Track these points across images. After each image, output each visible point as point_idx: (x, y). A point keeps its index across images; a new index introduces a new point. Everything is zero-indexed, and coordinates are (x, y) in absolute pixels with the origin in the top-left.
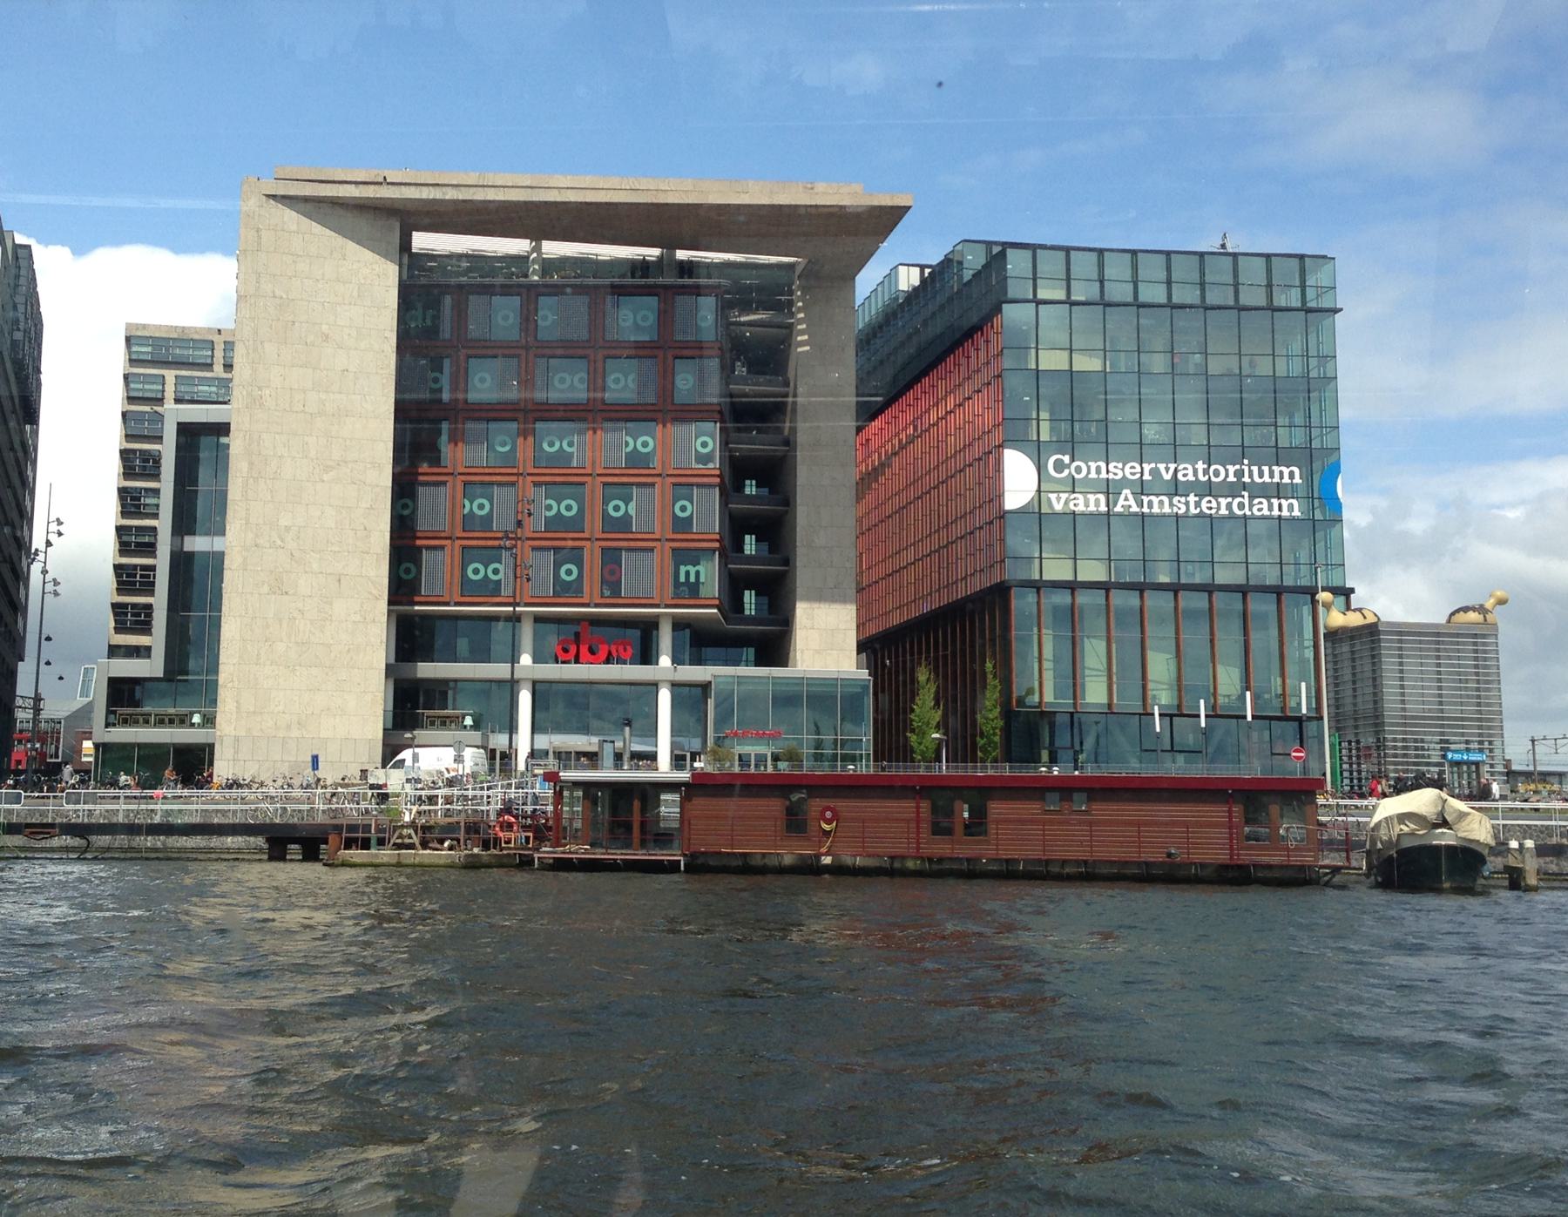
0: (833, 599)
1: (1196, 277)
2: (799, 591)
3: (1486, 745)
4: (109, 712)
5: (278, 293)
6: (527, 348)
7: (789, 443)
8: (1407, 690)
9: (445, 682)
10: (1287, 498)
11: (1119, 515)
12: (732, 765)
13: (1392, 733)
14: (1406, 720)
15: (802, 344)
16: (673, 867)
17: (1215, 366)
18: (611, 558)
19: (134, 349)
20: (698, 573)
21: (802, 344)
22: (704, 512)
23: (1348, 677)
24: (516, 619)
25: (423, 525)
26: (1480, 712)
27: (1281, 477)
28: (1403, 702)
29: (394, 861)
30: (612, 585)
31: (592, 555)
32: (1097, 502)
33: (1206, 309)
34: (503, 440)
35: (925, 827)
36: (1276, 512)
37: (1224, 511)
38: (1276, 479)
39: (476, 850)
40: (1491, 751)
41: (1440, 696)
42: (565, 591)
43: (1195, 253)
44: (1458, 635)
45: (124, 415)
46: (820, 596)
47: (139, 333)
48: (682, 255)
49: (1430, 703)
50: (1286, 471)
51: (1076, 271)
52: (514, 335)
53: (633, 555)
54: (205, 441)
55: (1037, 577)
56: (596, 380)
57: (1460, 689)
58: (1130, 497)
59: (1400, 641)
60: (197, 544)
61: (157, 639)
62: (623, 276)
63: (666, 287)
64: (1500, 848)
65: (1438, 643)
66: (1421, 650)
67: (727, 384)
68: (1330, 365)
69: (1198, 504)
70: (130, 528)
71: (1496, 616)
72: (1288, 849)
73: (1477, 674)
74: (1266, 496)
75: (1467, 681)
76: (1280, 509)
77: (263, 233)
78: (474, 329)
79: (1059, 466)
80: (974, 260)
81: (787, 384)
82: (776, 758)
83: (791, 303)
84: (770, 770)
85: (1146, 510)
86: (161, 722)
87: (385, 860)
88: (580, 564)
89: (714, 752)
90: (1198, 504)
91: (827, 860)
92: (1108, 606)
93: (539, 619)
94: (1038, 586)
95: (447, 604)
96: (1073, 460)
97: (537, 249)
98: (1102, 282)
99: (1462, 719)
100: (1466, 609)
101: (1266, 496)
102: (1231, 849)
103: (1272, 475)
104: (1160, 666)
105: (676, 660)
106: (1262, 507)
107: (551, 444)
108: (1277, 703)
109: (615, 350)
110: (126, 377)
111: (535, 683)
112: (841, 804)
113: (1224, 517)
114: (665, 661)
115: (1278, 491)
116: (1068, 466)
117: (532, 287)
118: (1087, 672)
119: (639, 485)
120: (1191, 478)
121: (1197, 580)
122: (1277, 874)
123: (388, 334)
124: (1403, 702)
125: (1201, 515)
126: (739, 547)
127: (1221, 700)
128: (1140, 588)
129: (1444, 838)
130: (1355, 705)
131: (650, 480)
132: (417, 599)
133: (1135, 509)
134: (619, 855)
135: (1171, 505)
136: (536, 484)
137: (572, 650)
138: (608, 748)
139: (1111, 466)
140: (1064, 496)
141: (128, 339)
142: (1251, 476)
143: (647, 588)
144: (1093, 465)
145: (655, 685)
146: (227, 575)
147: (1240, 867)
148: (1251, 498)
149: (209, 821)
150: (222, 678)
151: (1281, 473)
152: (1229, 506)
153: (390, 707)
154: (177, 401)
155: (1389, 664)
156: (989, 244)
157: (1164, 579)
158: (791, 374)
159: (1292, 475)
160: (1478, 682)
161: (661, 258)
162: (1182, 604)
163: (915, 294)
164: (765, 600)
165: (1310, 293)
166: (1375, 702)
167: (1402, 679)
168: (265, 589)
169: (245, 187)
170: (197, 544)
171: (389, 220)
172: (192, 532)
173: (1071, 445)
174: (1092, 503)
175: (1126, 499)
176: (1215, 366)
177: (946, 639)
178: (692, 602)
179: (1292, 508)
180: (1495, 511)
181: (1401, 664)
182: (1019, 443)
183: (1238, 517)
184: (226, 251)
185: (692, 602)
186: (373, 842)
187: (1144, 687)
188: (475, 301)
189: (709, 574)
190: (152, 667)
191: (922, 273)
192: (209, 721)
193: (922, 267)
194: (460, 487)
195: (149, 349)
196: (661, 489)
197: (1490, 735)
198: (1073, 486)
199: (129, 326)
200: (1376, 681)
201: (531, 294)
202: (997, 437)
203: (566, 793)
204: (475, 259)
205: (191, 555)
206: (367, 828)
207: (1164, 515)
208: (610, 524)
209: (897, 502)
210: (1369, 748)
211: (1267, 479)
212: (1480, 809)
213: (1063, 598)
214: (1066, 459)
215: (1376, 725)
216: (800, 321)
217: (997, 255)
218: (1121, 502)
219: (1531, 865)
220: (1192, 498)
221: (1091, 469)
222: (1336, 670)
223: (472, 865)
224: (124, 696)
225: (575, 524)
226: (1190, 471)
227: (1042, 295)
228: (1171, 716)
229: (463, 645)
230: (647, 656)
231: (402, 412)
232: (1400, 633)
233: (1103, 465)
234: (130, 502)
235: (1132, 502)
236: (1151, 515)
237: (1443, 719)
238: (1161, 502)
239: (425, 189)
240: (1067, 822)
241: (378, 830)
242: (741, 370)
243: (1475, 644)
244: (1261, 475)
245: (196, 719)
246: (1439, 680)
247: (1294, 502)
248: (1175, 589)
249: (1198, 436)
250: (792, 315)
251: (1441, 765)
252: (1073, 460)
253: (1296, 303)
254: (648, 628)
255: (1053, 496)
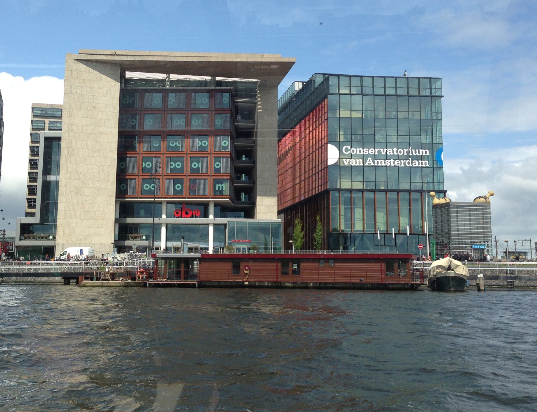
0: (269, 195)
1: (394, 85)
2: (258, 193)
3: (486, 243)
4: (21, 235)
5: (78, 93)
6: (164, 111)
7: (255, 142)
8: (459, 225)
9: (138, 224)
10: (424, 160)
11: (367, 166)
12: (234, 252)
13: (454, 239)
14: (459, 235)
15: (260, 109)
16: (194, 286)
17: (400, 116)
18: (193, 182)
19: (35, 112)
20: (222, 187)
21: (260, 109)
22: (225, 166)
23: (440, 220)
24: (161, 203)
25: (128, 171)
26: (484, 232)
27: (423, 153)
28: (458, 229)
29: (100, 285)
30: (193, 190)
31: (187, 183)
32: (360, 162)
33: (363, 95)
34: (156, 143)
35: (279, 272)
36: (420, 165)
37: (403, 165)
38: (421, 154)
39: (129, 281)
40: (488, 245)
41: (470, 226)
42: (178, 193)
43: (417, 78)
44: (477, 206)
45: (31, 134)
46: (266, 194)
47: (37, 107)
48: (218, 79)
49: (467, 229)
50: (424, 151)
51: (353, 83)
52: (160, 106)
53: (200, 181)
54: (55, 144)
55: (339, 188)
56: (188, 122)
57: (477, 224)
58: (371, 160)
59: (457, 208)
60: (52, 178)
61: (37, 210)
62: (198, 86)
63: (212, 90)
64: (473, 277)
65: (470, 209)
66: (464, 211)
67: (234, 123)
68: (439, 115)
69: (394, 163)
70: (33, 173)
71: (491, 199)
72: (400, 278)
73: (483, 219)
74: (416, 158)
75: (480, 221)
76: (422, 164)
77: (73, 72)
78: (147, 104)
79: (347, 150)
80: (319, 80)
81: (254, 123)
82: (249, 249)
83: (256, 95)
84: (247, 253)
85: (376, 164)
86: (38, 239)
87: (98, 284)
88: (182, 184)
89: (228, 247)
90: (394, 163)
91: (246, 283)
92: (363, 197)
93: (168, 203)
94: (339, 190)
95: (137, 198)
96: (351, 148)
97: (168, 77)
98: (373, 88)
99: (478, 234)
100: (480, 197)
101: (416, 158)
102: (381, 278)
103: (419, 152)
104: (381, 217)
105: (216, 216)
106: (416, 164)
107: (173, 144)
108: (420, 229)
109: (199, 112)
110: (32, 121)
111: (167, 225)
112: (250, 264)
113: (403, 167)
114: (211, 217)
115: (421, 158)
116: (350, 150)
117: (167, 90)
118: (356, 219)
119: (202, 157)
120: (392, 153)
121: (394, 188)
122: (396, 286)
123: (116, 106)
124: (458, 229)
125: (395, 166)
126: (239, 178)
127: (401, 229)
128: (374, 191)
129: (451, 274)
130: (442, 230)
131: (206, 155)
132: (126, 196)
133: (372, 164)
134: (175, 282)
135: (385, 163)
136: (167, 157)
137: (180, 213)
138: (186, 246)
139: (364, 150)
140: (348, 160)
141: (33, 108)
142: (412, 153)
143: (204, 192)
144: (358, 150)
145: (208, 225)
146: (60, 188)
147: (384, 284)
148: (412, 160)
149: (49, 272)
150: (58, 224)
151: (422, 152)
152: (405, 163)
153: (117, 232)
154: (50, 129)
155: (453, 216)
156: (324, 74)
157: (382, 188)
158: (256, 119)
159: (426, 152)
160: (483, 222)
161: (211, 80)
162: (388, 196)
163: (301, 91)
164: (247, 196)
165: (433, 91)
166: (448, 229)
167: (457, 221)
168: (73, 193)
169: (67, 57)
170: (52, 178)
171: (118, 68)
172: (50, 174)
173: (351, 143)
174: (358, 162)
175: (369, 161)
176: (400, 116)
177: (308, 210)
178: (220, 197)
179: (426, 164)
180: (511, 164)
181: (457, 216)
182: (333, 142)
183: (408, 167)
184: (60, 77)
185: (220, 197)
186: (95, 278)
187: (375, 224)
188: (147, 95)
189: (226, 187)
190: (35, 220)
191: (303, 84)
192: (54, 238)
193: (303, 82)
194: (141, 158)
195: (40, 112)
196: (210, 158)
197: (487, 240)
198: (351, 156)
199: (33, 104)
200: (449, 221)
201: (165, 92)
202: (326, 140)
203: (159, 261)
204: (147, 81)
205: (50, 182)
206: (92, 274)
207: (383, 166)
208: (192, 170)
209: (295, 162)
210: (446, 244)
211: (417, 154)
212: (464, 264)
213: (348, 195)
214: (349, 147)
215: (449, 236)
216: (259, 101)
217: (327, 77)
218: (368, 162)
219: (482, 283)
220: (392, 161)
221: (357, 151)
222: (436, 218)
223: (127, 286)
224: (26, 230)
225: (181, 170)
226: (391, 151)
227: (342, 91)
228: (384, 234)
229: (142, 212)
230: (206, 215)
231: (121, 134)
232: (457, 206)
233: (361, 149)
234: (33, 164)
235: (371, 162)
236: (378, 166)
237: (471, 234)
238: (381, 162)
239: (129, 57)
240: (326, 270)
241: (97, 274)
242: (239, 118)
243: (483, 209)
244: (416, 152)
245: (51, 237)
246: (470, 221)
247: (427, 162)
248: (386, 191)
249: (394, 139)
250: (256, 99)
251: (471, 250)
252: (351, 148)
253: (428, 94)
254: (206, 206)
255: (344, 160)
